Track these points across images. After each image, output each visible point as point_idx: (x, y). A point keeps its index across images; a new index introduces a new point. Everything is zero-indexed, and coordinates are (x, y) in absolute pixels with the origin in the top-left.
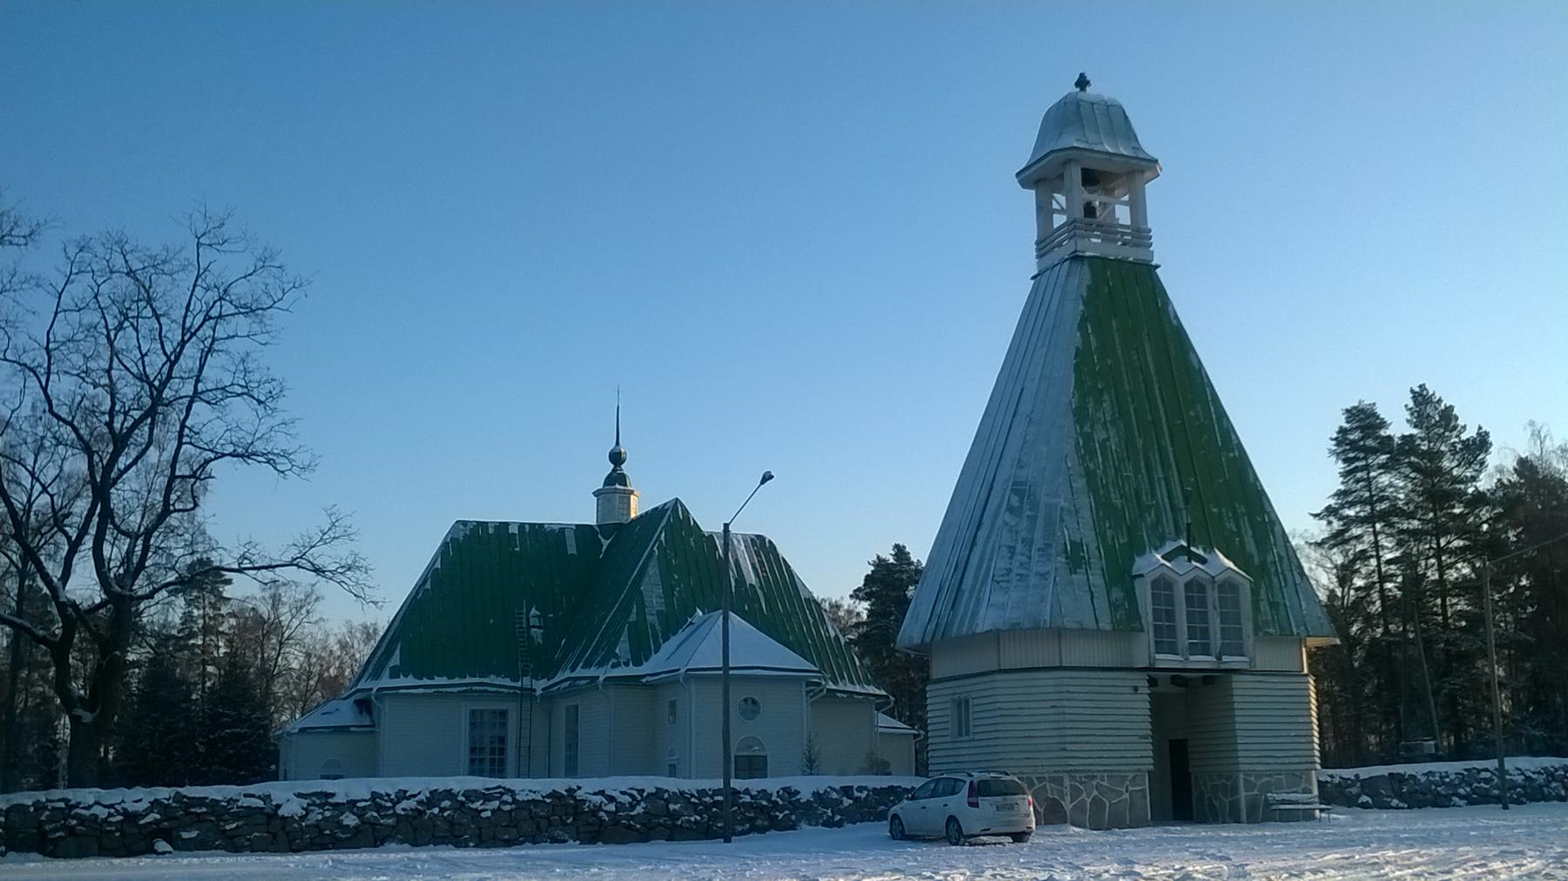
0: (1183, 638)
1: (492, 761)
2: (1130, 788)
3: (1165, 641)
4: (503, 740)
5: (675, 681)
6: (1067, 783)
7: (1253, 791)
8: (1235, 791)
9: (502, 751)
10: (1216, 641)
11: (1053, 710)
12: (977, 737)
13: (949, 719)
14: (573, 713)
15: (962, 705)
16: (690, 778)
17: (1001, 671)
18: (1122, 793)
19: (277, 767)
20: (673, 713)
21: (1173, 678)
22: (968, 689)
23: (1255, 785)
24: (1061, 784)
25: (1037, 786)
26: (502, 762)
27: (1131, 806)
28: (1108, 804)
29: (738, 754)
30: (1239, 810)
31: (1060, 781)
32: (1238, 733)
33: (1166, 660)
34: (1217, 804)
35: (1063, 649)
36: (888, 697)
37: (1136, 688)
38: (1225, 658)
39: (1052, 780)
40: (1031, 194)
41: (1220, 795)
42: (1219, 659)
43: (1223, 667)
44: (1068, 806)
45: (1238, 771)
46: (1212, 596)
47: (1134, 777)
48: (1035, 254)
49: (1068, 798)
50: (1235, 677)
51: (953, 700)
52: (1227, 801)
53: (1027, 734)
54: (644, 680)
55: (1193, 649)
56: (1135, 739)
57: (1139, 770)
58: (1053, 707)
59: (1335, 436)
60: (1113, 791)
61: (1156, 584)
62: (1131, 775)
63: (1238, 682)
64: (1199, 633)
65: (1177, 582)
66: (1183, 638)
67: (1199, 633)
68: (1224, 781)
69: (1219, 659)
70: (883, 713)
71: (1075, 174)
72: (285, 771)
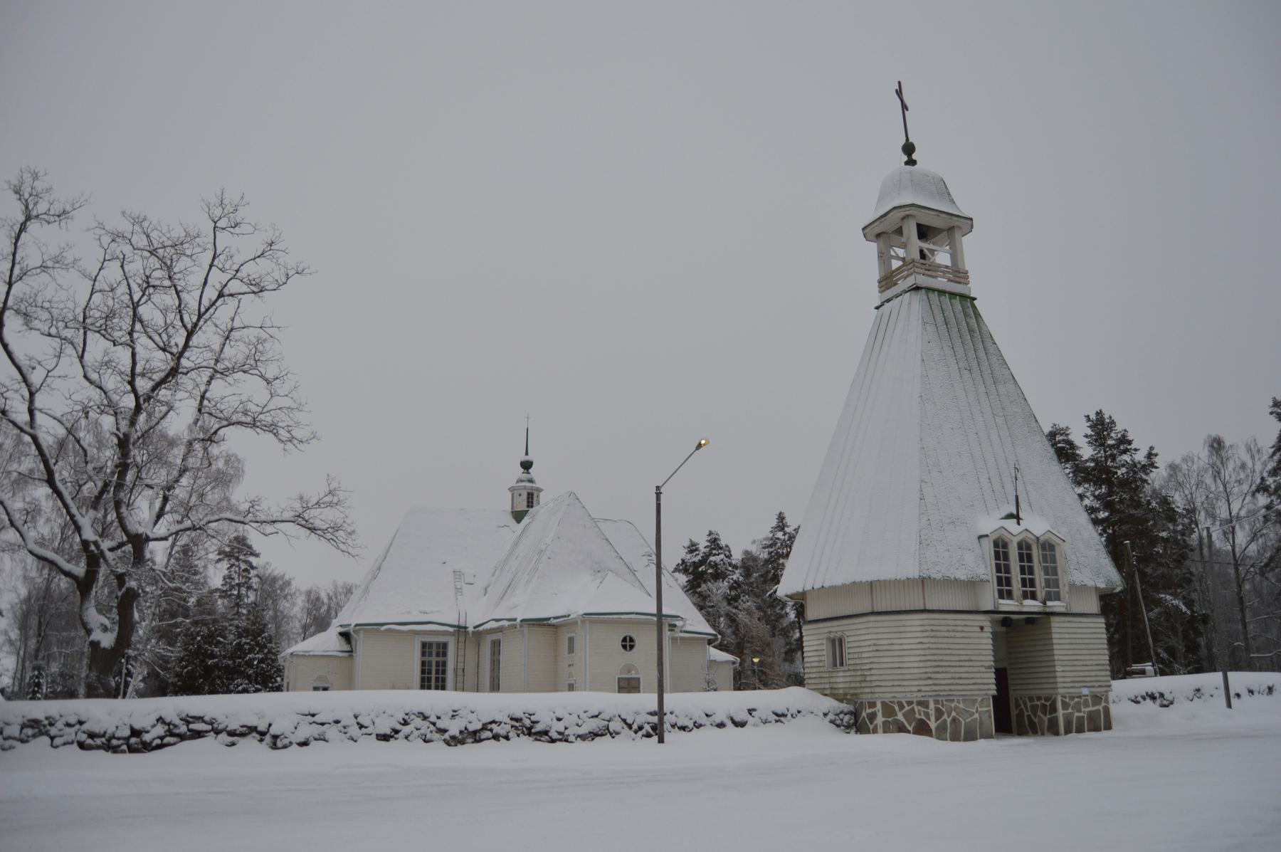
0: (1017, 587)
1: (437, 679)
2: (979, 709)
3: (1005, 594)
4: (444, 664)
5: (575, 623)
6: (932, 705)
7: (1067, 709)
8: (1054, 709)
9: (444, 672)
10: (1040, 590)
11: (920, 646)
12: (851, 668)
13: (825, 653)
14: (496, 645)
15: (837, 644)
16: (585, 690)
17: (873, 613)
18: (973, 713)
19: (282, 680)
20: (571, 650)
21: (1005, 618)
22: (845, 628)
23: (1072, 709)
24: (927, 707)
25: (907, 708)
26: (444, 680)
27: (981, 724)
28: (963, 722)
29: (620, 676)
30: (1057, 725)
31: (923, 704)
32: (1057, 663)
33: (1007, 605)
34: (1036, 720)
35: (926, 595)
36: (717, 635)
37: (982, 628)
38: (1049, 603)
39: (919, 703)
40: (873, 247)
41: (1039, 713)
42: (1044, 603)
43: (1048, 610)
44: (933, 724)
45: (1057, 694)
46: (1036, 553)
47: (982, 700)
48: (878, 289)
49: (933, 718)
50: (1053, 619)
51: (828, 639)
52: (1046, 719)
53: (897, 665)
54: (383, 628)
55: (1025, 596)
56: (983, 669)
57: (986, 694)
58: (919, 643)
59: (340, 583)
60: (967, 711)
61: (1020, 546)
62: (980, 699)
63: (1056, 623)
64: (1028, 583)
65: (1011, 541)
66: (1017, 587)
67: (1028, 583)
68: (1043, 702)
69: (1044, 603)
70: (714, 647)
71: (911, 231)
72: (288, 683)
